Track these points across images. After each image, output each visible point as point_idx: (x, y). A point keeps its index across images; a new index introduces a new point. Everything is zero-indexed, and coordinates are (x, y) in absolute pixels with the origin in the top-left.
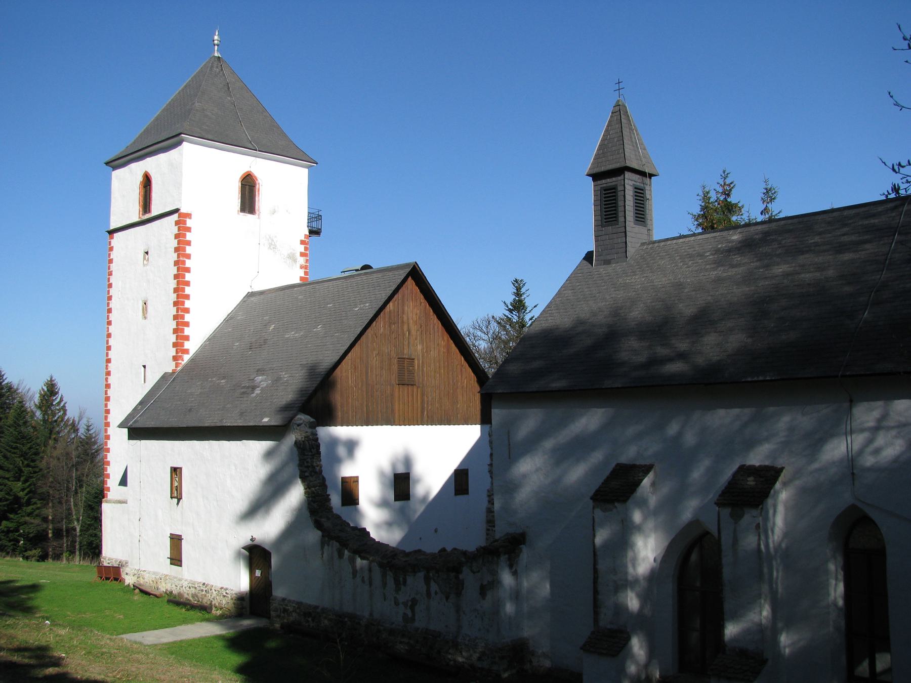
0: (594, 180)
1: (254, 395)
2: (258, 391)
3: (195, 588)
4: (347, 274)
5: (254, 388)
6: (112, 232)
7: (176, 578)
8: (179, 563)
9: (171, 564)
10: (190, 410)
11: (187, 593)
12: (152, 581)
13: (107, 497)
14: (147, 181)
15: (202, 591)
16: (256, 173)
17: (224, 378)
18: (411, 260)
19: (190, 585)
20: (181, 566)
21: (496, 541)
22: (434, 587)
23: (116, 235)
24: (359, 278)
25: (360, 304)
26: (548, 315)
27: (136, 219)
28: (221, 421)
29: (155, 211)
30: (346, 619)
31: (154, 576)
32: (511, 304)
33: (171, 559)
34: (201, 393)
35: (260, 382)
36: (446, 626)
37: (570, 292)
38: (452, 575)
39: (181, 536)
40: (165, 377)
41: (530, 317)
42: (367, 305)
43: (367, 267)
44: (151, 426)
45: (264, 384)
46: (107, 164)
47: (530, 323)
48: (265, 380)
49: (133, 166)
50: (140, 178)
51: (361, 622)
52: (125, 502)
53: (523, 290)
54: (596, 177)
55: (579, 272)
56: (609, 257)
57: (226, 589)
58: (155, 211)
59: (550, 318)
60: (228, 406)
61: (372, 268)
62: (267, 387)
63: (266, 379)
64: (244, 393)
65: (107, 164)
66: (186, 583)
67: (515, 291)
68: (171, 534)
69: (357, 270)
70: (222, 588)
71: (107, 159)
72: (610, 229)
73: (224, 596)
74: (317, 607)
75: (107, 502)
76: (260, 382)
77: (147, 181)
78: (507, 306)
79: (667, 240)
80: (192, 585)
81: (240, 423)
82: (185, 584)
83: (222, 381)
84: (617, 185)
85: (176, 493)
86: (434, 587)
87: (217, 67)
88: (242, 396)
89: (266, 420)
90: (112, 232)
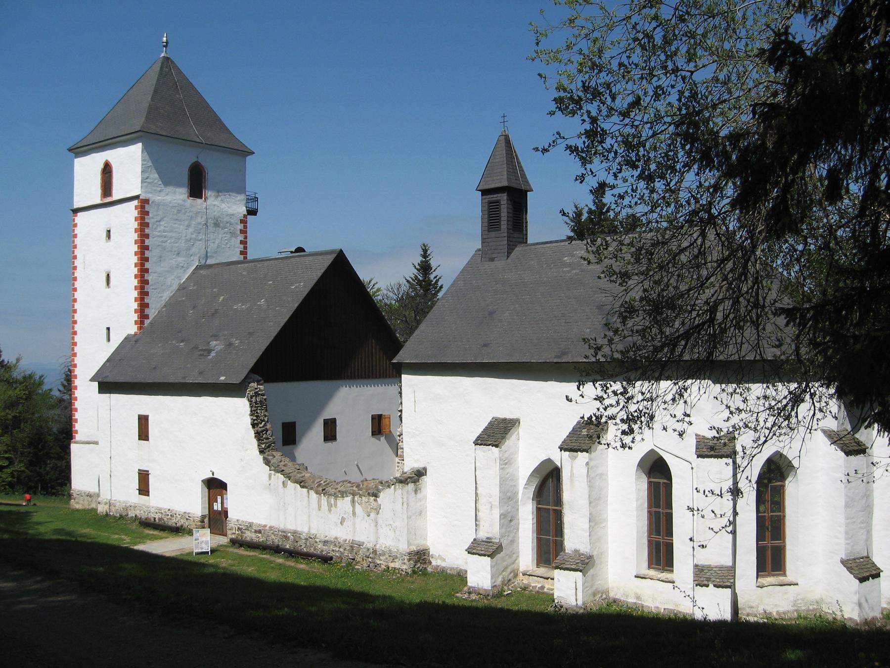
0: (482, 195)
1: (210, 357)
2: (213, 354)
3: (162, 513)
4: (283, 255)
5: (209, 351)
6: (76, 211)
7: (144, 505)
8: (147, 494)
9: (139, 494)
10: (155, 368)
11: (153, 516)
12: (123, 508)
13: (75, 439)
14: (107, 170)
15: (168, 515)
16: (202, 161)
17: (182, 342)
18: (337, 246)
19: (156, 511)
20: (148, 495)
21: (406, 473)
22: (358, 508)
23: (79, 214)
24: (293, 260)
25: (296, 283)
26: (445, 301)
27: (98, 201)
28: (184, 378)
29: (116, 195)
30: (289, 534)
31: (124, 504)
32: (419, 264)
33: (139, 490)
34: (162, 354)
35: (215, 346)
36: (368, 537)
37: (462, 282)
38: (372, 498)
39: (148, 471)
40: (128, 339)
41: (435, 276)
42: (302, 284)
43: (300, 250)
44: (121, 381)
45: (219, 348)
46: (70, 150)
47: (434, 281)
48: (219, 344)
49: (94, 156)
50: (101, 166)
51: (301, 536)
52: (96, 443)
53: (429, 252)
54: (484, 192)
55: (470, 266)
56: (494, 256)
57: (189, 513)
58: (116, 195)
59: (446, 304)
60: (189, 365)
61: (304, 251)
62: (221, 350)
63: (219, 344)
64: (201, 355)
65: (70, 150)
66: (154, 509)
67: (422, 253)
68: (139, 470)
69: (292, 252)
70: (185, 513)
71: (69, 145)
72: (493, 234)
73: (187, 519)
74: (265, 526)
75: (75, 443)
76: (215, 346)
77: (107, 170)
78: (415, 267)
79: (537, 244)
80: (159, 511)
81: (200, 380)
82: (153, 510)
83: (182, 344)
84: (500, 200)
85: (144, 435)
86: (358, 508)
87: (167, 67)
88: (200, 357)
89: (223, 378)
90: (76, 211)
